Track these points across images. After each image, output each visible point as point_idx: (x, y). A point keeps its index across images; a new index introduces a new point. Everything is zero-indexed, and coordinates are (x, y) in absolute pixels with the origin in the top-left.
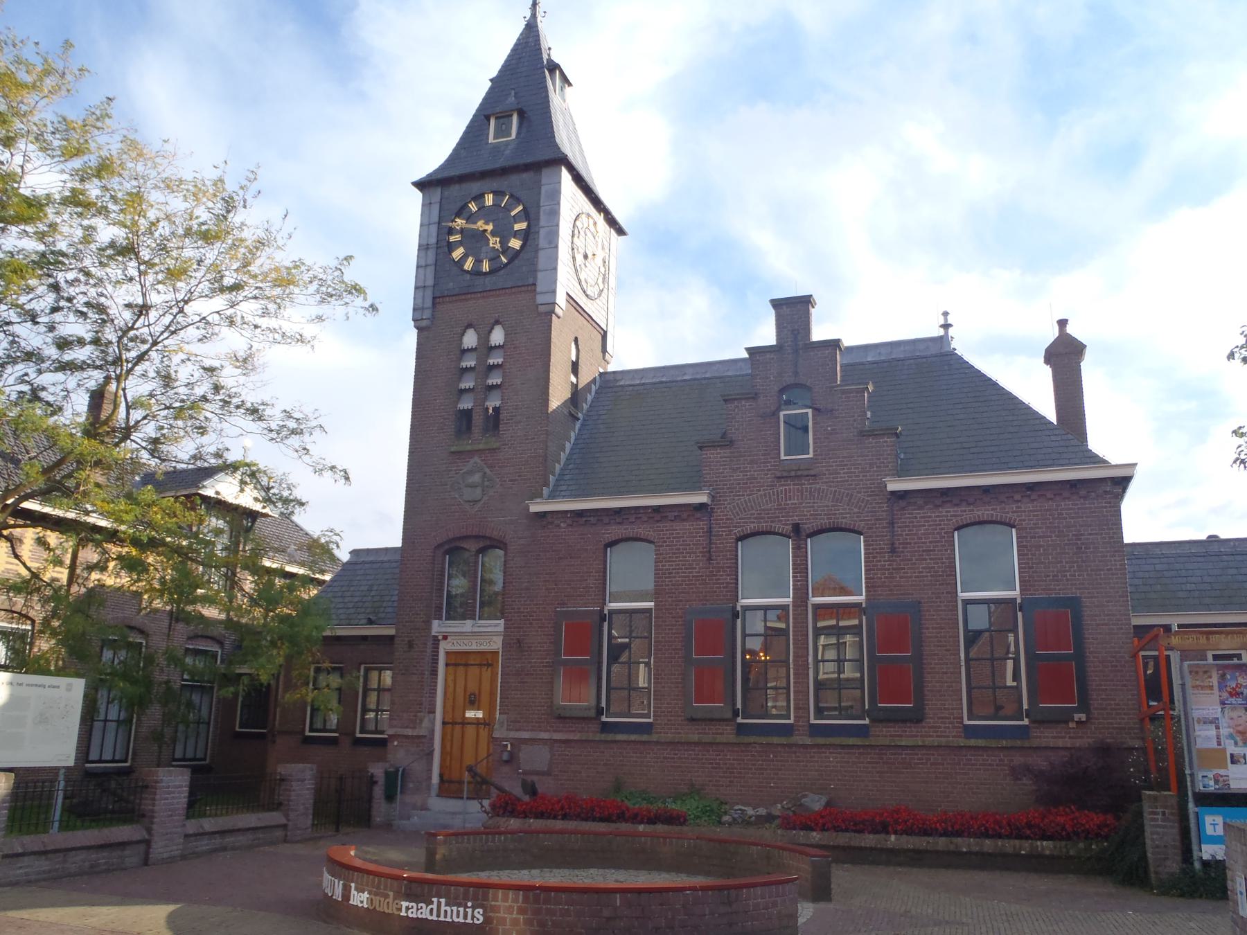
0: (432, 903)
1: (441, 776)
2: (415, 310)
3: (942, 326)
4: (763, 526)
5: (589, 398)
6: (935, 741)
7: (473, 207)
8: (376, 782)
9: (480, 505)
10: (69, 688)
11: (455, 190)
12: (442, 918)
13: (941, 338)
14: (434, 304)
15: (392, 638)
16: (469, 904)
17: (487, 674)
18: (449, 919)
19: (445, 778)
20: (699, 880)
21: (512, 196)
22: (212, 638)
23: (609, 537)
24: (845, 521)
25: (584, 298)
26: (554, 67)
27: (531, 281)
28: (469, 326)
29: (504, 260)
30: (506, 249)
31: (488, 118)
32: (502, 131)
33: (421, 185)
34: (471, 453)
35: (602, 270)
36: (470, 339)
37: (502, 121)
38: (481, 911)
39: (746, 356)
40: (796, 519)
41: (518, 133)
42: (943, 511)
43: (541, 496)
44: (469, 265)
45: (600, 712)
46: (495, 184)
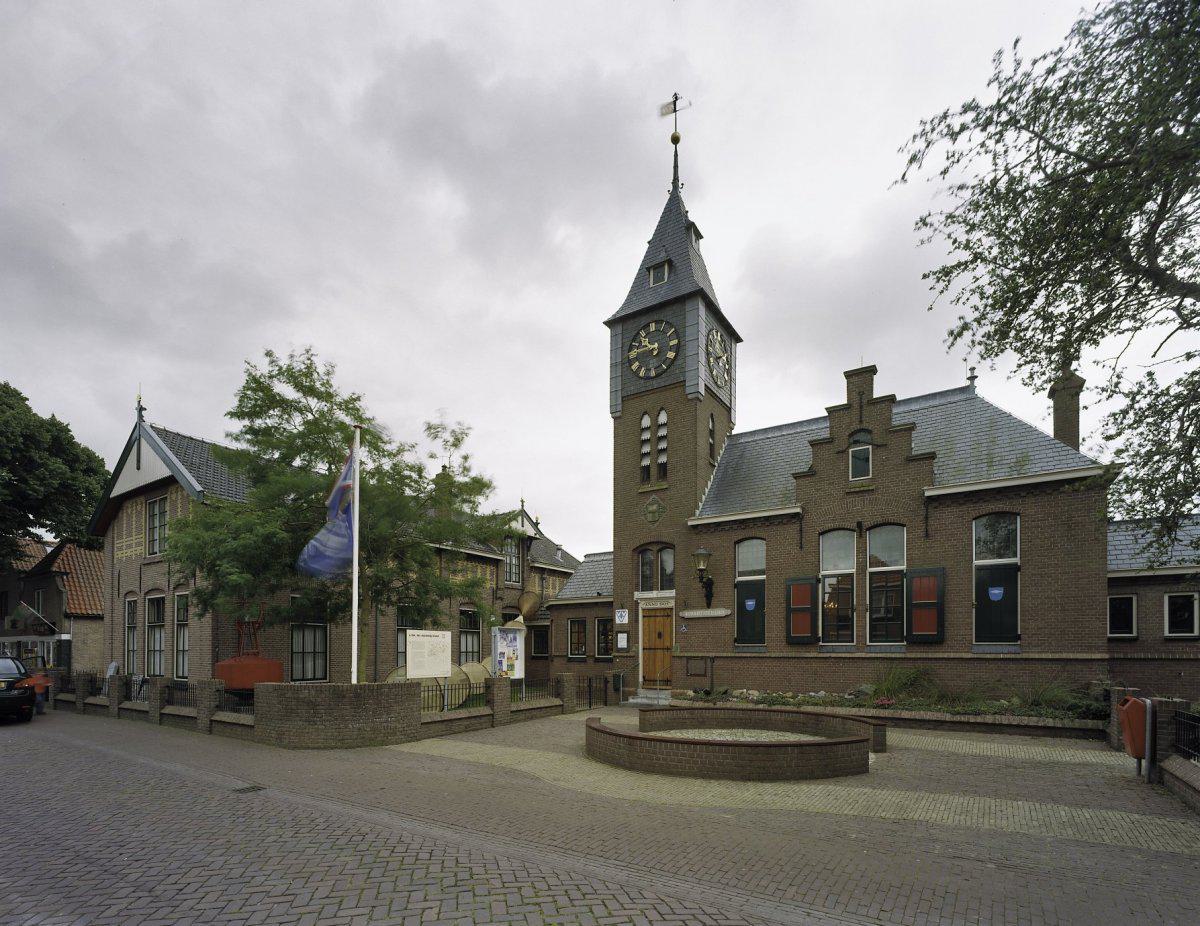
4: (837, 524)
14: (623, 401)
21: (667, 323)
22: (513, 607)
24: (892, 519)
36: (646, 422)
42: (964, 507)
44: (642, 374)
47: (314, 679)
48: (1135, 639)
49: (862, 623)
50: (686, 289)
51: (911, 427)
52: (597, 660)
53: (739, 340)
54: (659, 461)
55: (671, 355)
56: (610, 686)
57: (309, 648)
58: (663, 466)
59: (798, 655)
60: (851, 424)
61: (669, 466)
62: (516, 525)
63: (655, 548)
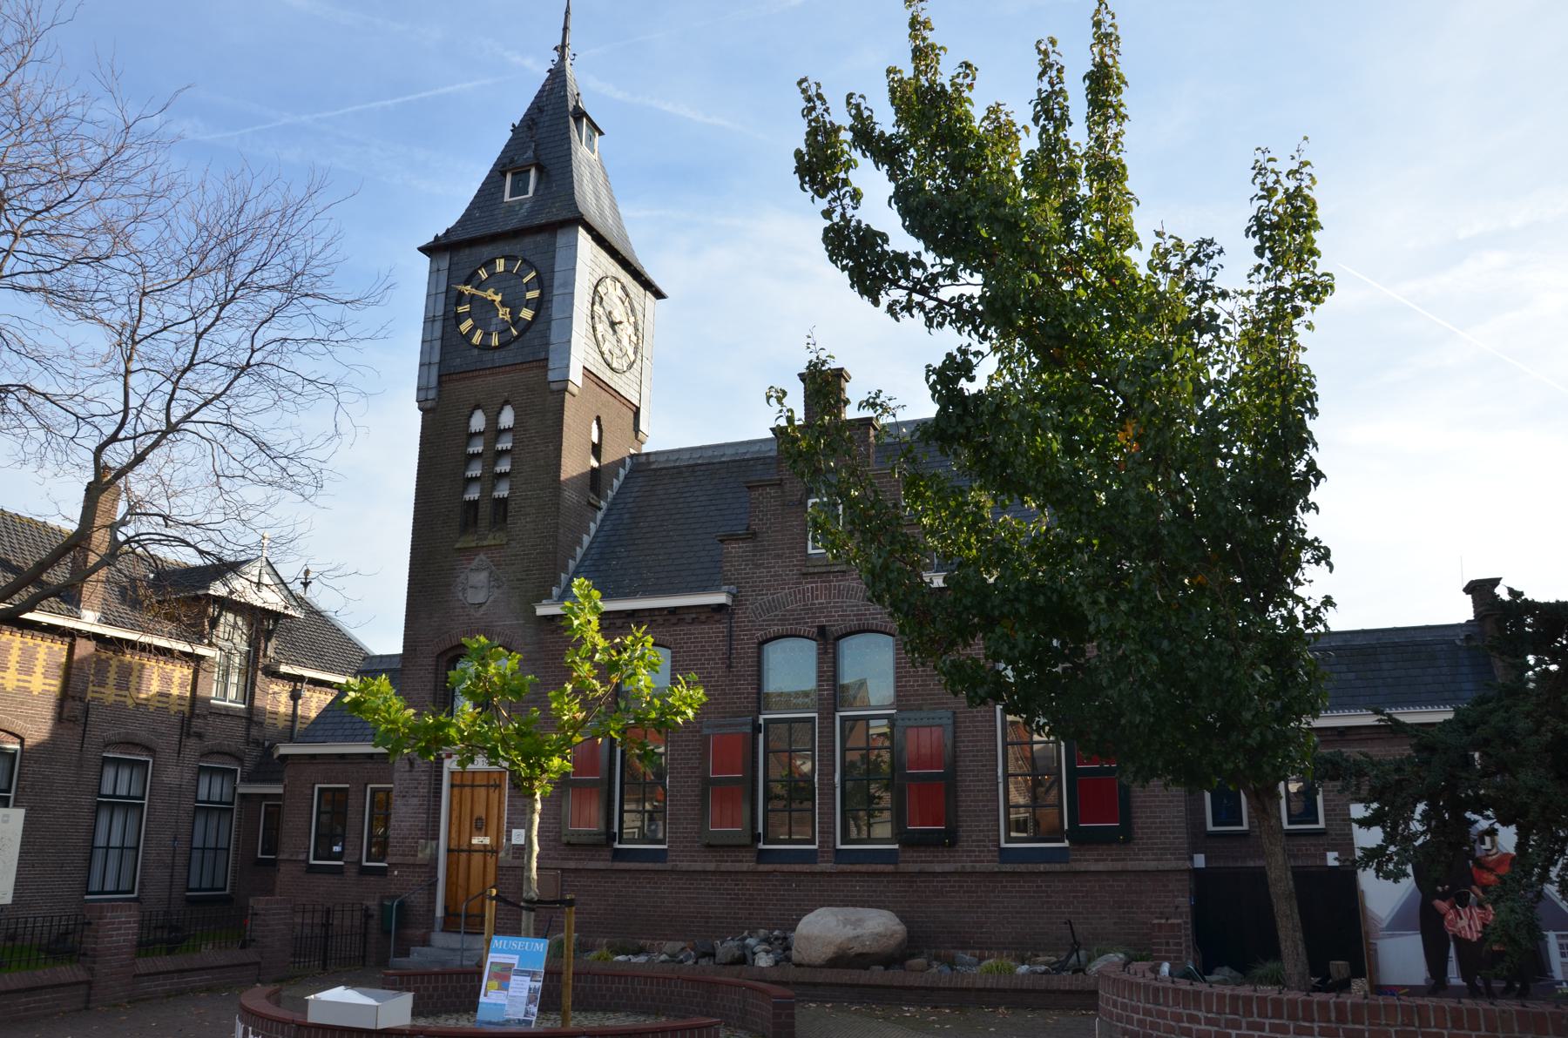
1: (446, 908)
5: (616, 483)
7: (483, 274)
11: (465, 255)
14: (440, 383)
17: (494, 796)
20: (663, 1021)
21: (524, 261)
22: (230, 754)
25: (609, 372)
26: (580, 114)
27: (542, 356)
28: (477, 407)
29: (515, 332)
30: (516, 320)
31: (504, 175)
32: (519, 188)
34: (478, 549)
35: (634, 338)
36: (478, 422)
41: (536, 190)
43: (549, 596)
45: (611, 837)
46: (507, 248)
47: (102, 892)
54: (496, 494)
56: (373, 924)
57: (115, 841)
59: (725, 867)
61: (512, 506)
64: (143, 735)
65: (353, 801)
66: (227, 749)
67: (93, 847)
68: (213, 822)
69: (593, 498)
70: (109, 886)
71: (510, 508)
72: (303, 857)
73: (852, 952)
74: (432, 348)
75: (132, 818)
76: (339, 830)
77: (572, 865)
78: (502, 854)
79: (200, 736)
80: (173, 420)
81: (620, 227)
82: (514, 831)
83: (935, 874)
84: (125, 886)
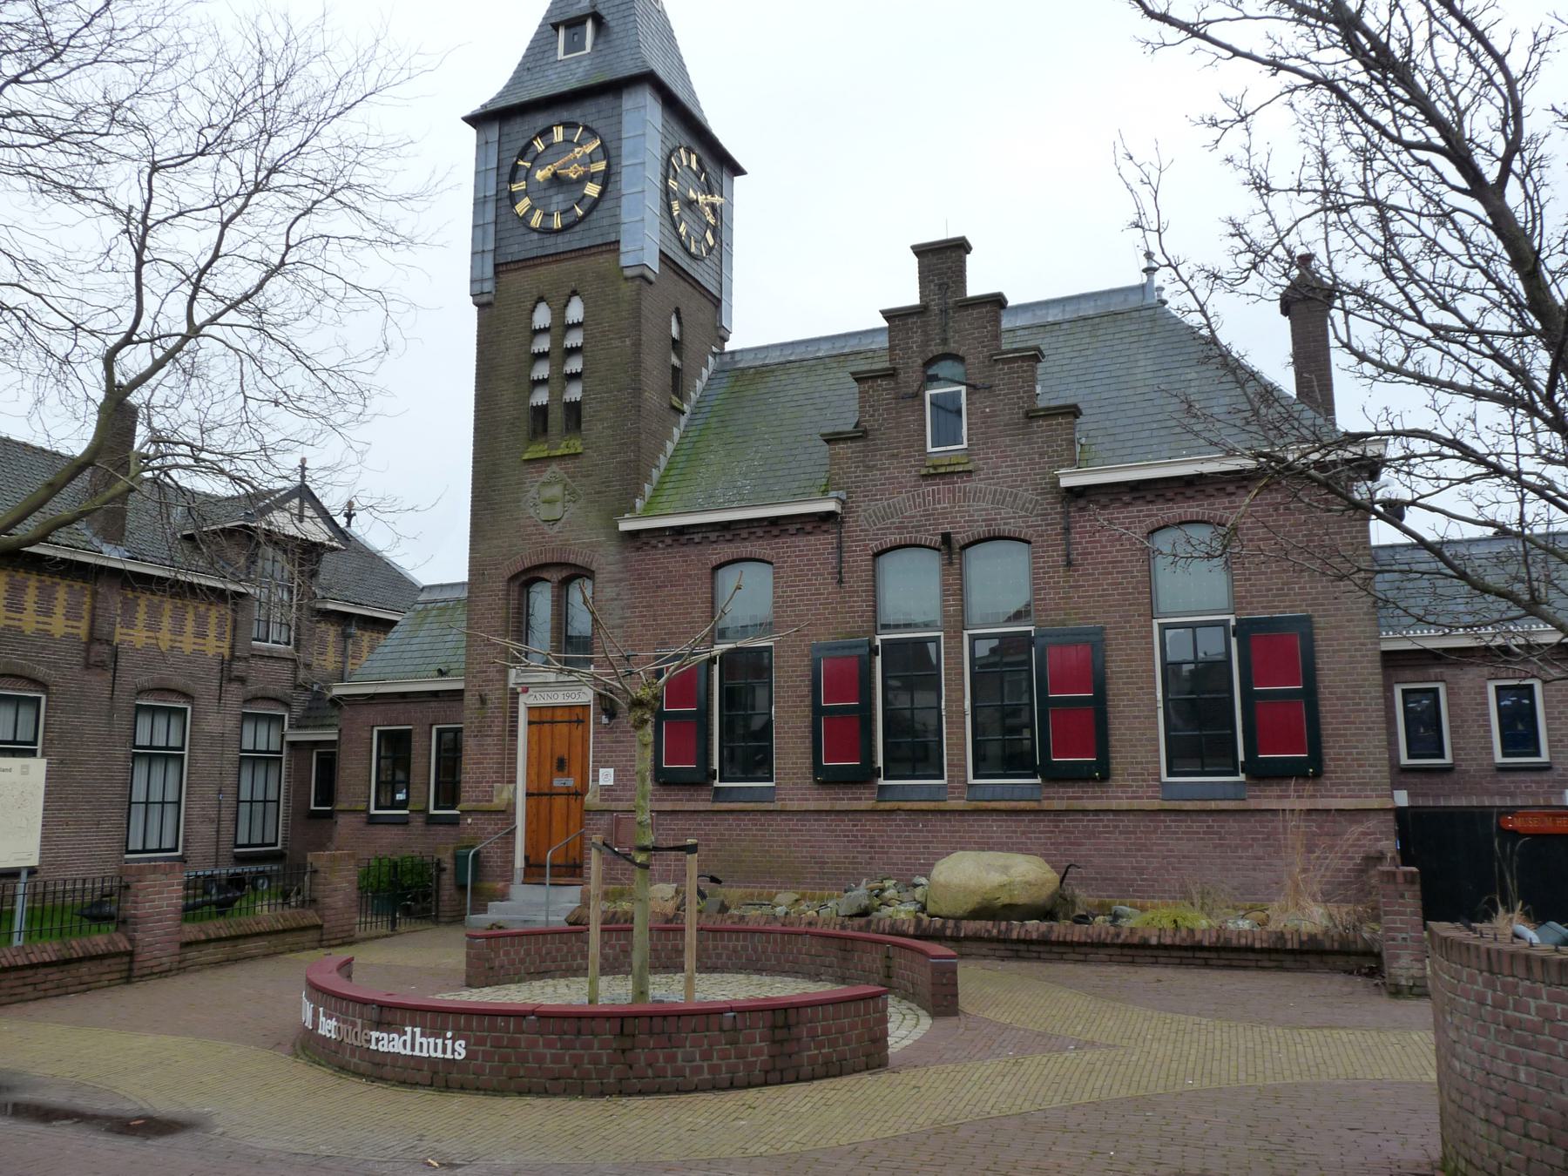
0: (405, 1033)
1: (527, 858)
2: (472, 281)
3: (1145, 271)
4: (906, 537)
6: (1125, 804)
8: (444, 869)
9: (559, 524)
10: (25, 771)
12: (417, 1053)
13: (1143, 287)
14: (496, 273)
15: (460, 692)
16: (449, 1034)
17: (577, 732)
18: (425, 1054)
19: (531, 861)
21: (586, 128)
22: (275, 700)
23: (715, 559)
24: (1006, 530)
25: (688, 260)
28: (541, 299)
33: (474, 120)
36: (542, 317)
37: (573, 30)
38: (463, 1043)
39: (885, 324)
40: (948, 528)
41: (594, 45)
42: (1133, 511)
44: (536, 221)
46: (566, 115)
47: (144, 851)
48: (1446, 770)
49: (959, 741)
50: (626, 68)
51: (1036, 356)
52: (432, 821)
53: (737, 170)
55: (592, 190)
58: (574, 409)
59: (839, 806)
60: (925, 343)
61: (586, 412)
62: (282, 521)
63: (556, 576)
64: (179, 682)
65: (417, 744)
66: (272, 694)
67: (130, 803)
68: (260, 774)
69: (675, 401)
70: (153, 843)
71: (583, 413)
72: (362, 807)
73: (999, 903)
74: (484, 233)
75: (173, 769)
76: (400, 776)
77: (668, 806)
78: (588, 797)
79: (242, 680)
80: (197, 322)
81: (692, 93)
82: (602, 771)
83: (1084, 812)
84: (167, 844)
